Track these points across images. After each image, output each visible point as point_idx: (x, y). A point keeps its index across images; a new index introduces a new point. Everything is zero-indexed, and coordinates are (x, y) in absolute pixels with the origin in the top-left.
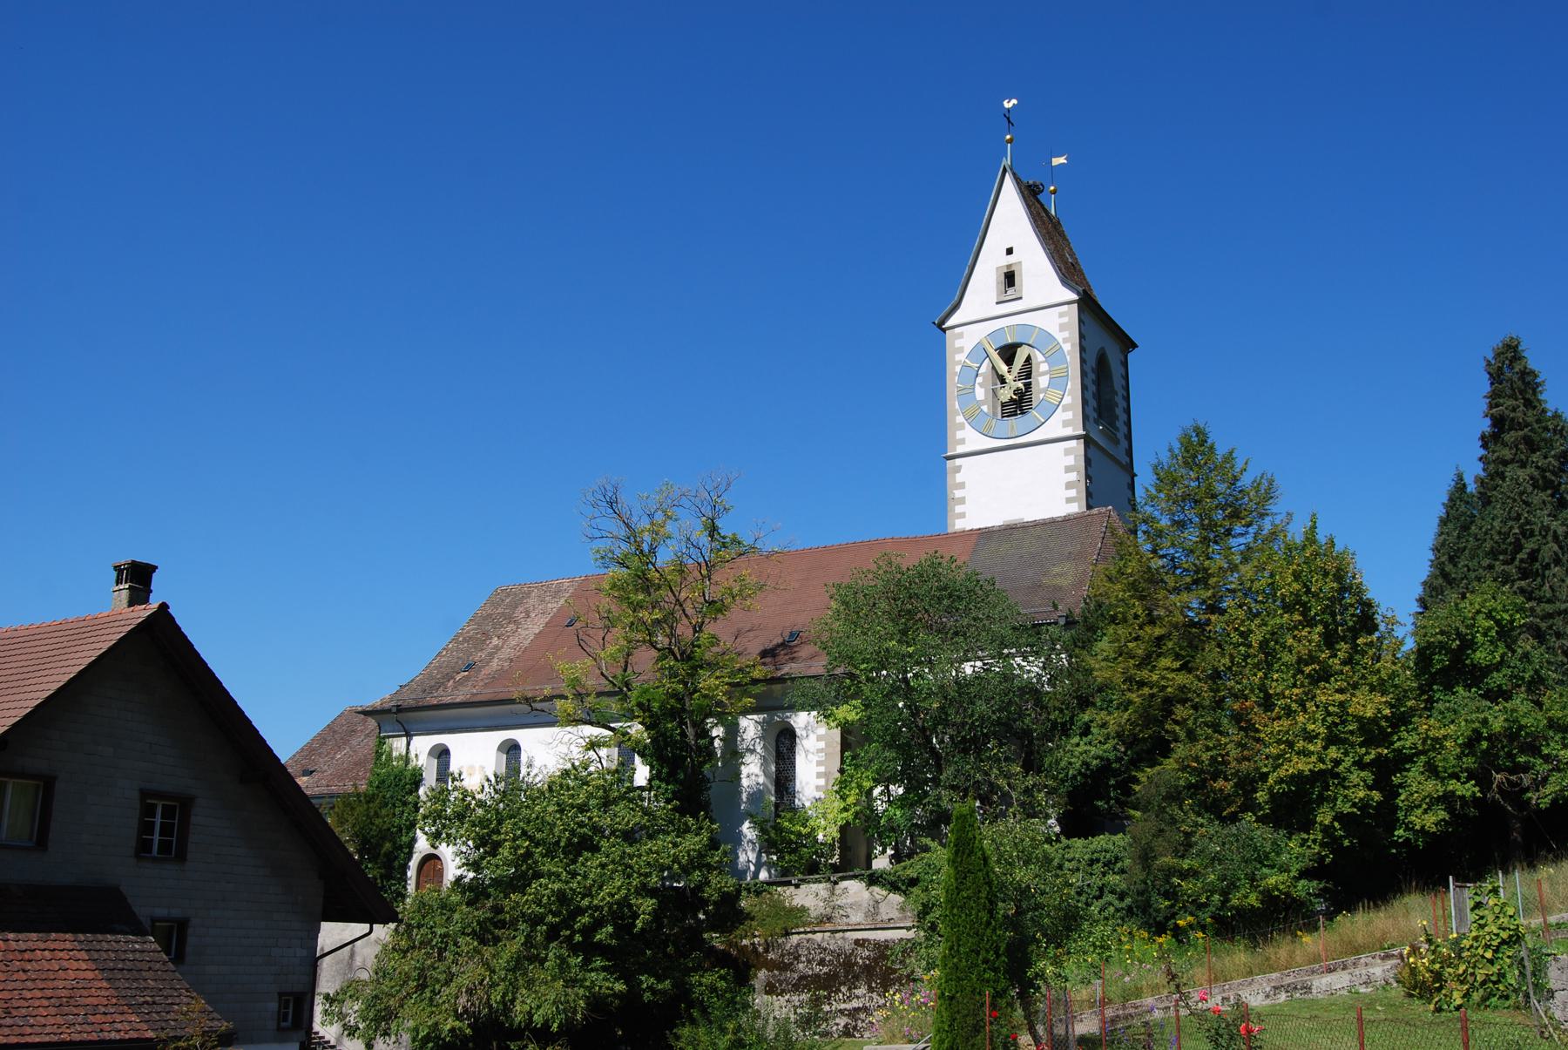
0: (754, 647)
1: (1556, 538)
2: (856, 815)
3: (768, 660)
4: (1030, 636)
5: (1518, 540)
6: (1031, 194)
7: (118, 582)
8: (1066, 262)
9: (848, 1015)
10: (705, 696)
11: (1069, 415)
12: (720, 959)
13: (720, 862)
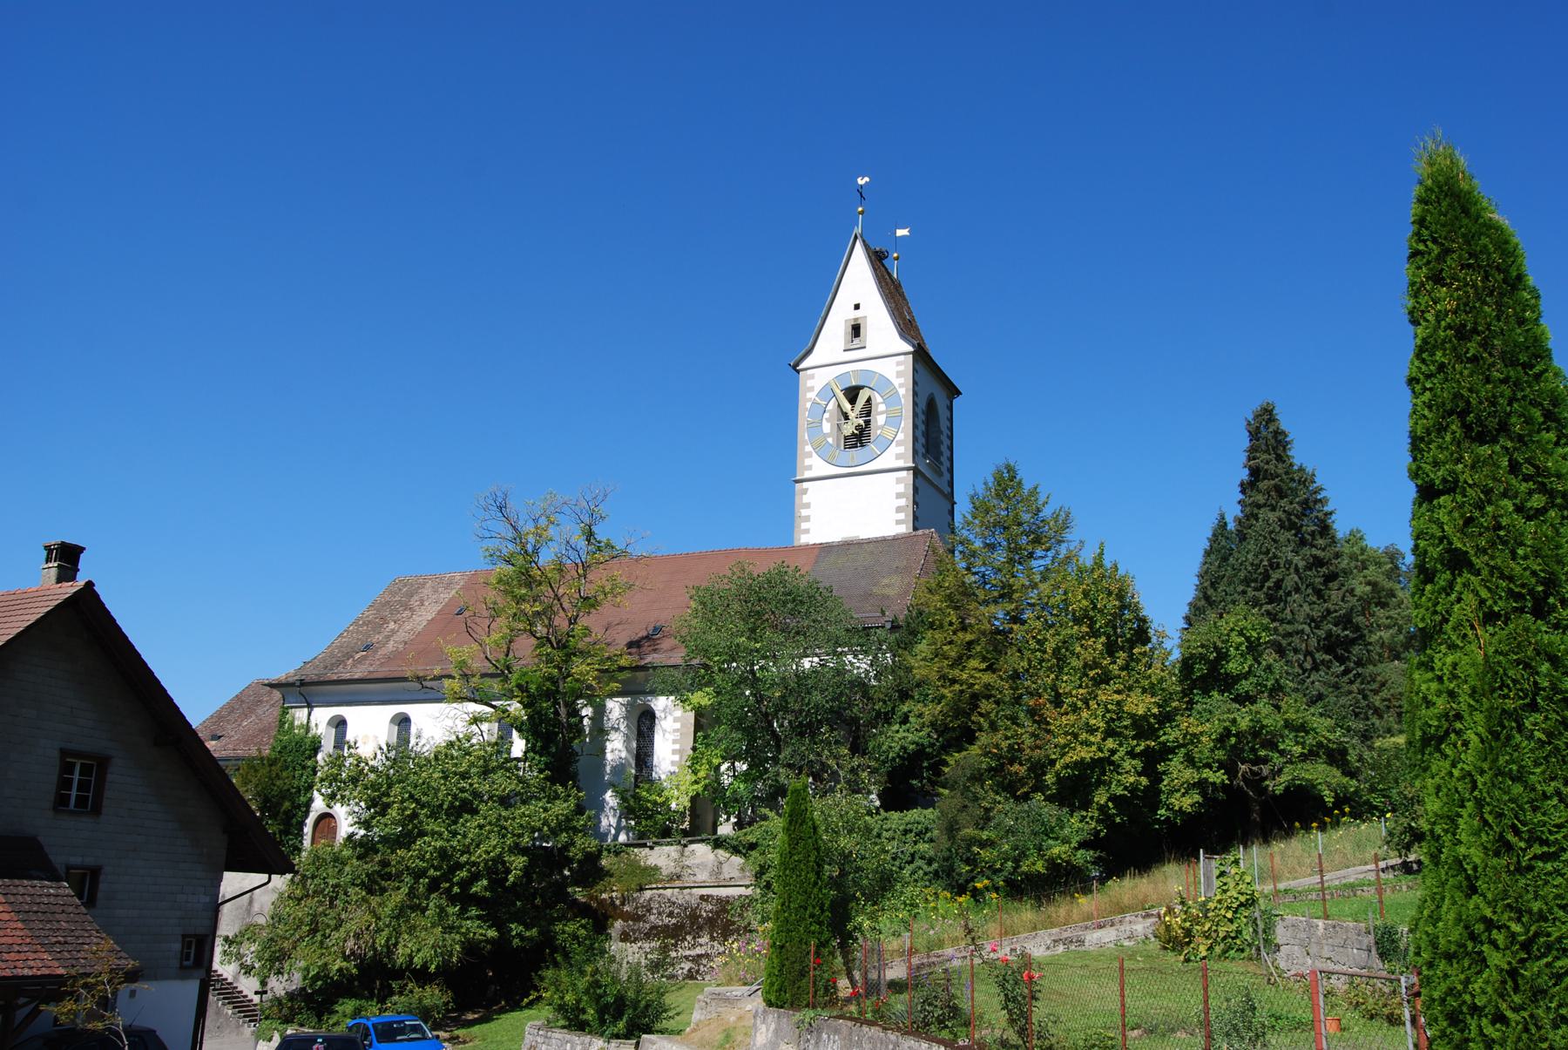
0: (622, 639)
1: (1297, 570)
2: (706, 787)
3: (633, 650)
6: (878, 259)
7: (48, 560)
8: (904, 319)
9: (692, 961)
11: (901, 449)
12: (583, 910)
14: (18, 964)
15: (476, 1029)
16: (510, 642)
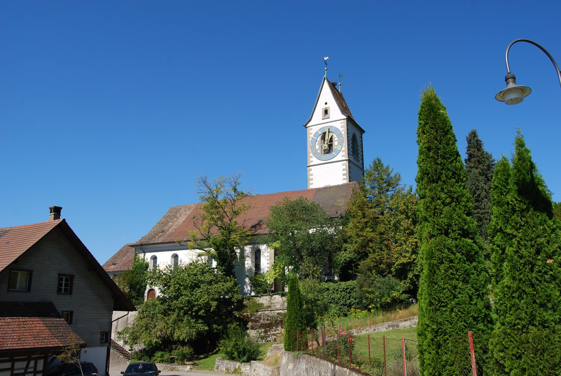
0: (250, 225)
1: (485, 190)
2: (279, 275)
3: (253, 229)
4: (329, 221)
5: (474, 191)
6: (333, 86)
7: (51, 212)
8: (343, 107)
10: (233, 240)
11: (344, 153)
12: (239, 319)
13: (237, 290)
14: (47, 343)
15: (202, 361)
16: (209, 228)
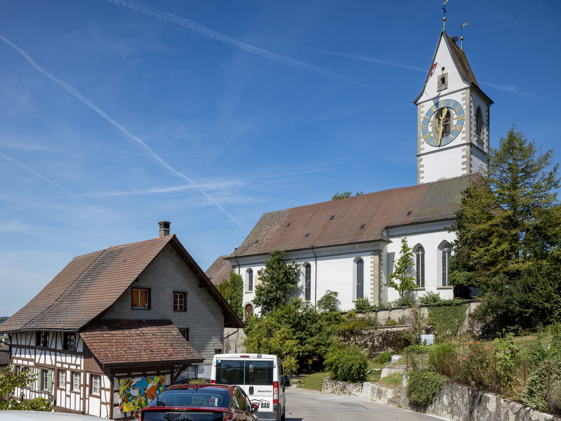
6: (453, 43)
11: (464, 135)
